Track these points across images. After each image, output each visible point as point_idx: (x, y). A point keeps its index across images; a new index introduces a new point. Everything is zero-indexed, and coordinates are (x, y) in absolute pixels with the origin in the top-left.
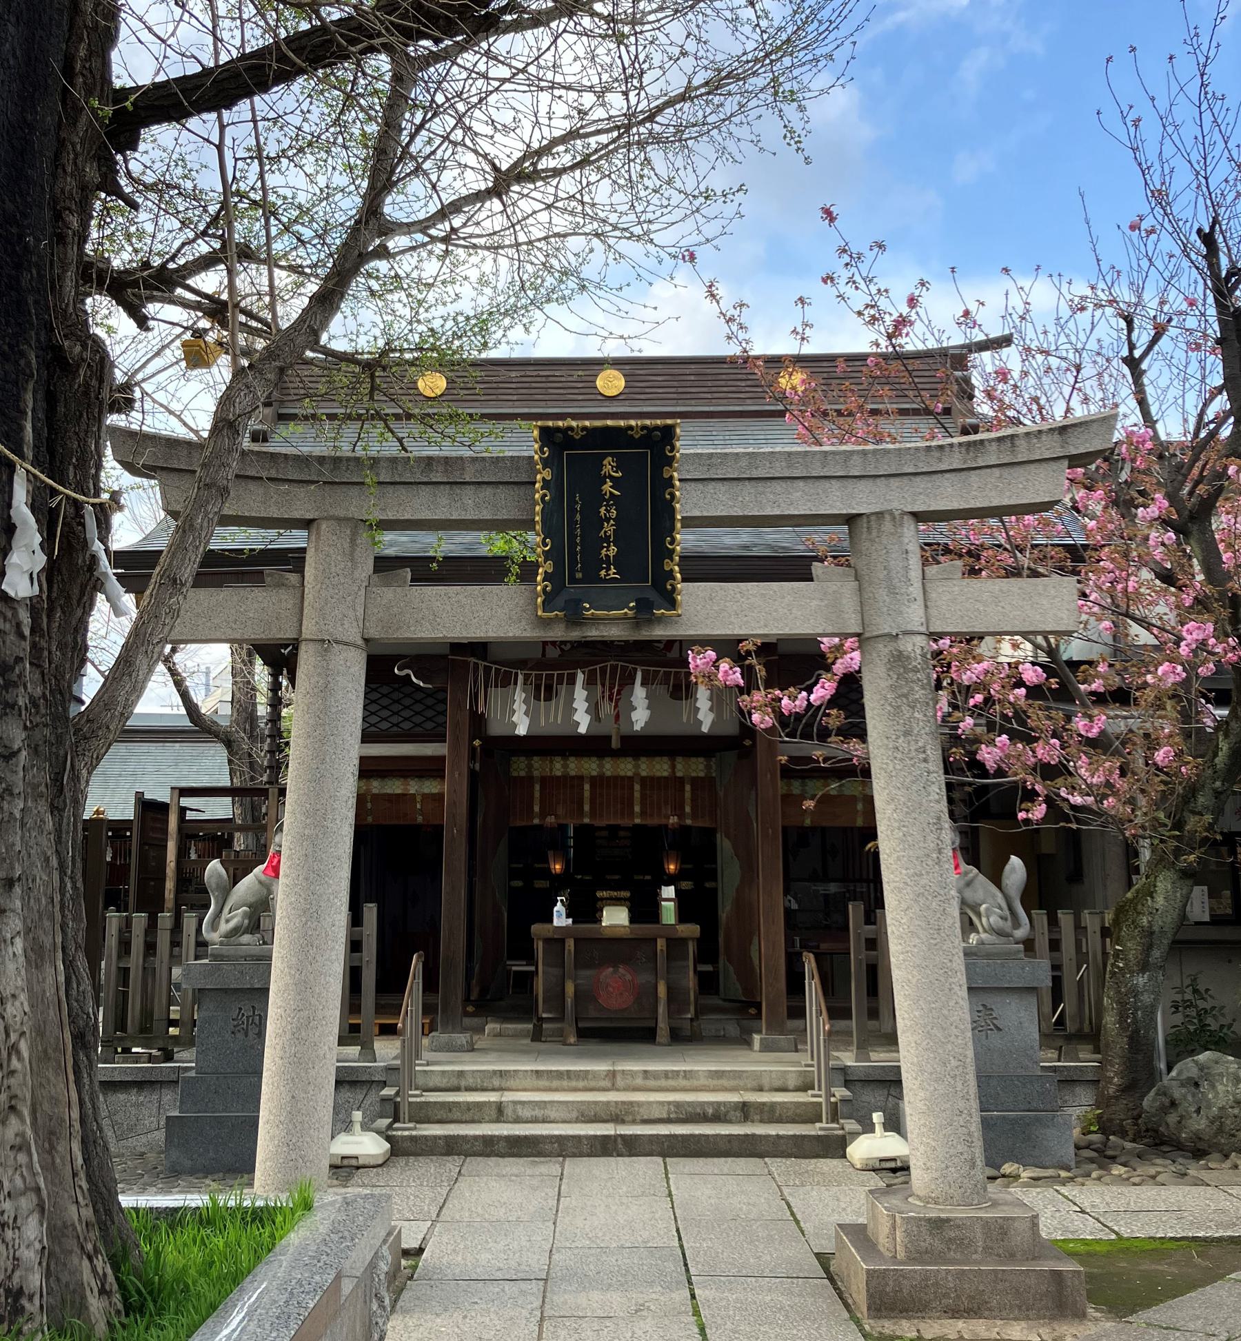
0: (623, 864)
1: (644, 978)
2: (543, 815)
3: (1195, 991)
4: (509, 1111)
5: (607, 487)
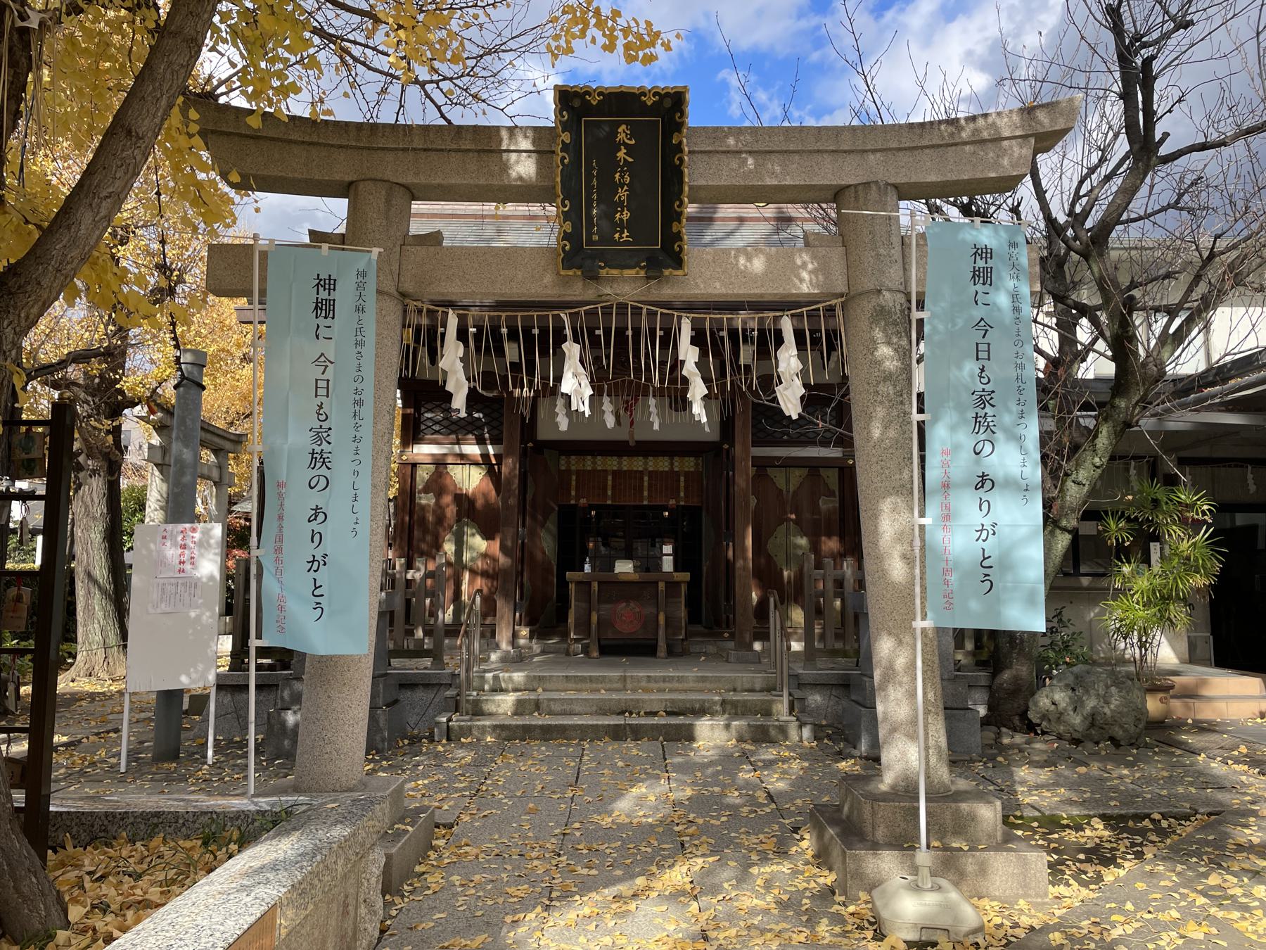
0: (637, 529)
1: (649, 610)
2: (578, 497)
3: (1060, 621)
4: (544, 706)
5: (621, 154)
